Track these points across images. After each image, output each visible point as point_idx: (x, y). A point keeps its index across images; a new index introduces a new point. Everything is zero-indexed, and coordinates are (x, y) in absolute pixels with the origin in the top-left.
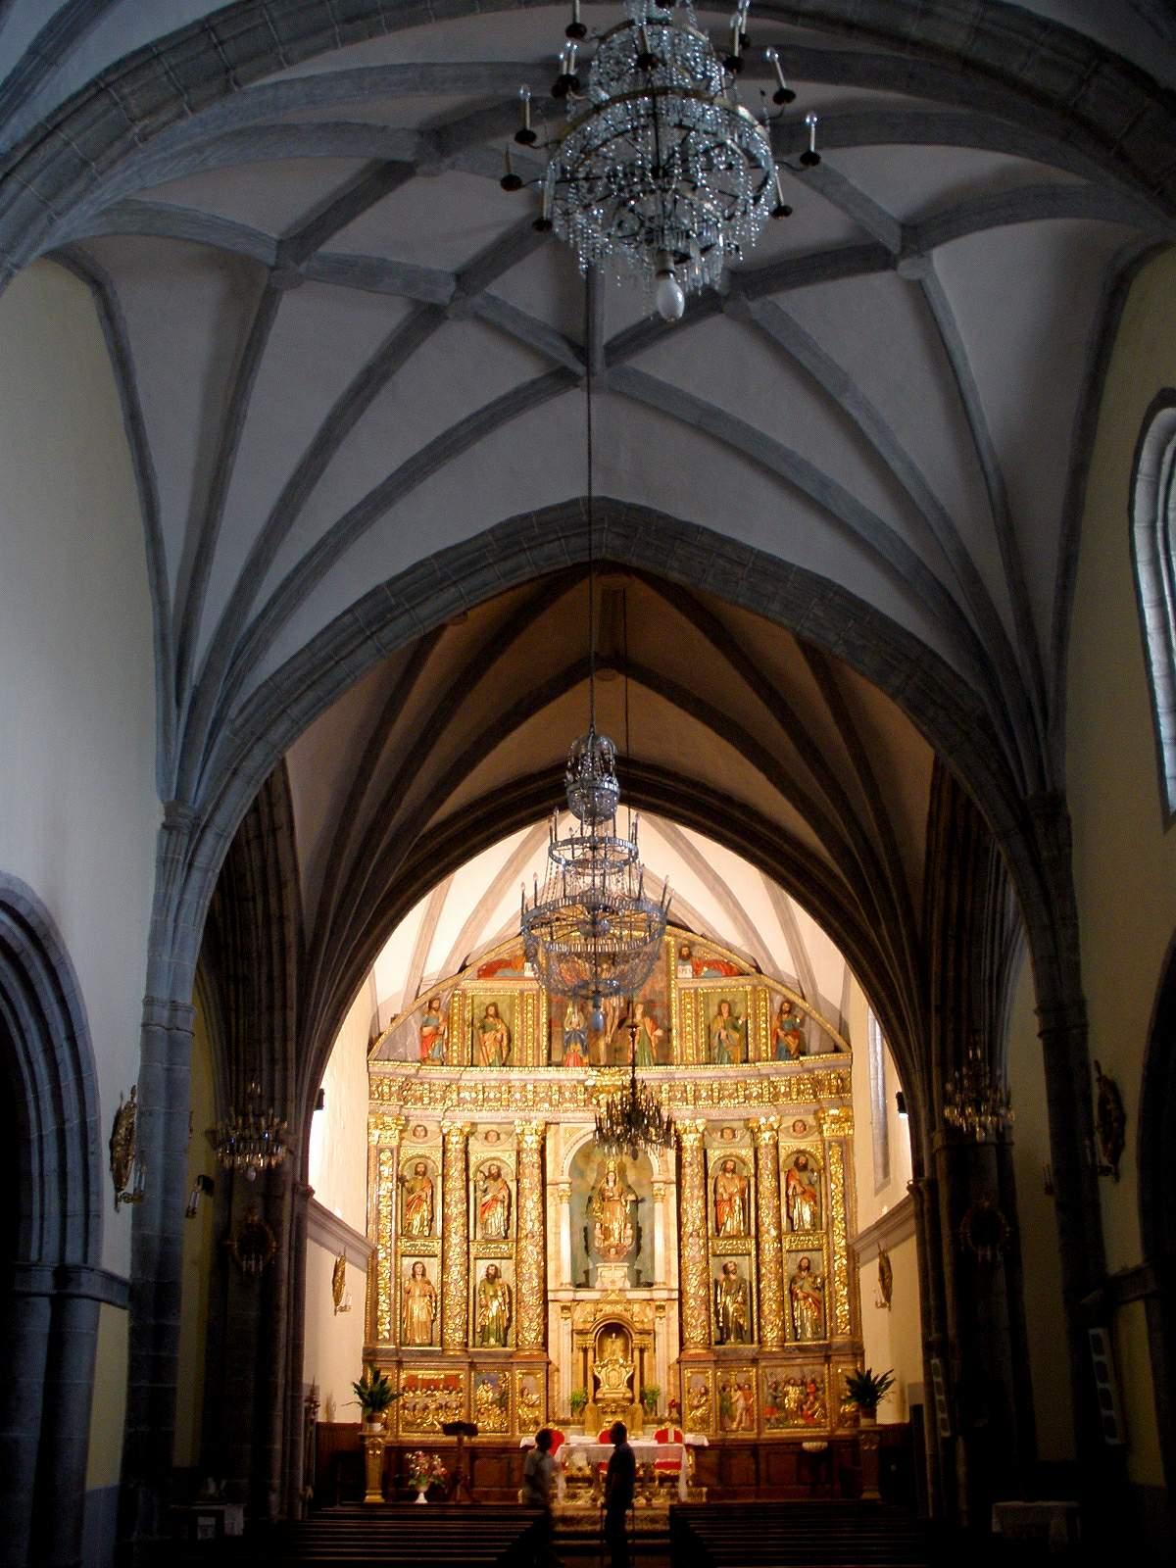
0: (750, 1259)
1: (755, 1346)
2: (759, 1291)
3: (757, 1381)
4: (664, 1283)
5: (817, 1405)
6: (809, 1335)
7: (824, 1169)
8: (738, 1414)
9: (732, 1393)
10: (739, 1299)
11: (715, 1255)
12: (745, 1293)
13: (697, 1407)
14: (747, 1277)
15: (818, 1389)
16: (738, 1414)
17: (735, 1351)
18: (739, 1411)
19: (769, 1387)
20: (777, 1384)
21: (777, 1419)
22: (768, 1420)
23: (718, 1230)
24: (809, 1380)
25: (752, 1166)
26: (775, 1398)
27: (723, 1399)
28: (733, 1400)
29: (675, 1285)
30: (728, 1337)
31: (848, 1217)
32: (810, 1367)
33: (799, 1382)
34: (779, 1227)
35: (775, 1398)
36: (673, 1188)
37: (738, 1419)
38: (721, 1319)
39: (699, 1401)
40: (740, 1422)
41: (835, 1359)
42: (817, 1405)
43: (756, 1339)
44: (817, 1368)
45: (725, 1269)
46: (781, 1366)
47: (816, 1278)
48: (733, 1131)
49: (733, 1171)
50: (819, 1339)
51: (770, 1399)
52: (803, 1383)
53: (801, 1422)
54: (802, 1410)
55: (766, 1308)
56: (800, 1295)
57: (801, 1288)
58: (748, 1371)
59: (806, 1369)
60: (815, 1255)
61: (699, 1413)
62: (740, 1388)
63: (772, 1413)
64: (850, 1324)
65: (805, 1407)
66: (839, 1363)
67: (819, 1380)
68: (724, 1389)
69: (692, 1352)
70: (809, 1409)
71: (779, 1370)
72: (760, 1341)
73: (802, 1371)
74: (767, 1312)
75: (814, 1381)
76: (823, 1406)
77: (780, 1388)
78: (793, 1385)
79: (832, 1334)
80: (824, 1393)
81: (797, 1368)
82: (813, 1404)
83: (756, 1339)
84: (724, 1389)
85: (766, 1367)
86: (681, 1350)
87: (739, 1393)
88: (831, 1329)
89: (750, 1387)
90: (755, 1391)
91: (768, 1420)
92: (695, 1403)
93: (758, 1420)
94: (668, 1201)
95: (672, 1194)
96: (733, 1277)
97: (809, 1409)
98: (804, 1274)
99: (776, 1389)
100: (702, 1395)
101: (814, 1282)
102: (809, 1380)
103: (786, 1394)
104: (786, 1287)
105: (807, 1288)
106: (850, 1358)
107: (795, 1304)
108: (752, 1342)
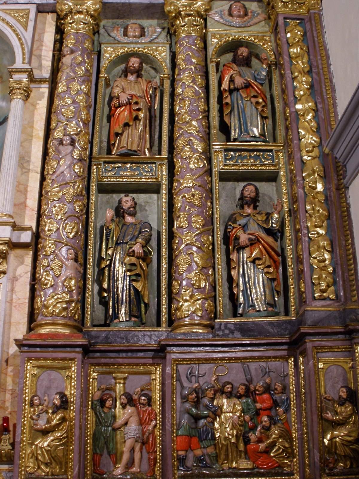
0: (159, 199)
1: (163, 329)
2: (171, 236)
3: (163, 391)
4: (10, 216)
5: (275, 432)
6: (260, 306)
7: (277, 65)
8: (126, 449)
9: (118, 411)
10: (137, 249)
11: (104, 189)
12: (148, 241)
13: (45, 433)
14: (154, 226)
15: (276, 404)
16: (126, 449)
17: (125, 336)
18: (129, 443)
19: (185, 399)
20: (199, 393)
21: (199, 460)
22: (182, 461)
23: (109, 152)
24: (259, 385)
25: (166, 65)
26: (196, 418)
27: (99, 422)
28: (120, 421)
29: (30, 221)
30: (116, 316)
31: (321, 114)
32: (263, 364)
33: (242, 390)
34: (207, 139)
35: (196, 418)
36: (45, 89)
37: (125, 457)
38: (105, 286)
39: (49, 421)
40: (131, 463)
41: (310, 343)
42: (275, 432)
43: (164, 318)
44: (275, 364)
45: (119, 212)
46: (207, 361)
47: (269, 215)
48: (142, 29)
49: (138, 73)
50: (277, 314)
51: (185, 420)
52: (248, 393)
53: (245, 464)
54: (247, 441)
55: (182, 261)
56: (244, 238)
57: (244, 227)
58: (149, 373)
59: (253, 366)
60: (265, 187)
61: (45, 443)
62: (130, 401)
63: (189, 448)
64: (335, 283)
65: (253, 437)
66: (319, 349)
67: (279, 386)
68: (102, 402)
69: (45, 330)
70: (260, 441)
71: (205, 368)
72: (170, 322)
73: (247, 371)
74: (184, 267)
75: (268, 389)
76: (286, 435)
77: (206, 401)
78: (229, 396)
79: (302, 301)
80: (287, 410)
81: (238, 365)
82: (268, 429)
83: (164, 318)
84: (102, 402)
85: (178, 362)
86: (30, 329)
87: (130, 410)
88: (301, 293)
89: (150, 402)
90: (157, 408)
91: (182, 461)
92: (42, 424)
93: (164, 459)
94: (34, 105)
95: (41, 98)
96: (129, 219)
97: (260, 441)
98: (248, 210)
99: (197, 403)
100: (56, 409)
101: (267, 220)
102: (259, 385)
103: (217, 412)
104: (219, 228)
105: (254, 229)
106: (338, 341)
107: (234, 256)
108: (159, 325)
